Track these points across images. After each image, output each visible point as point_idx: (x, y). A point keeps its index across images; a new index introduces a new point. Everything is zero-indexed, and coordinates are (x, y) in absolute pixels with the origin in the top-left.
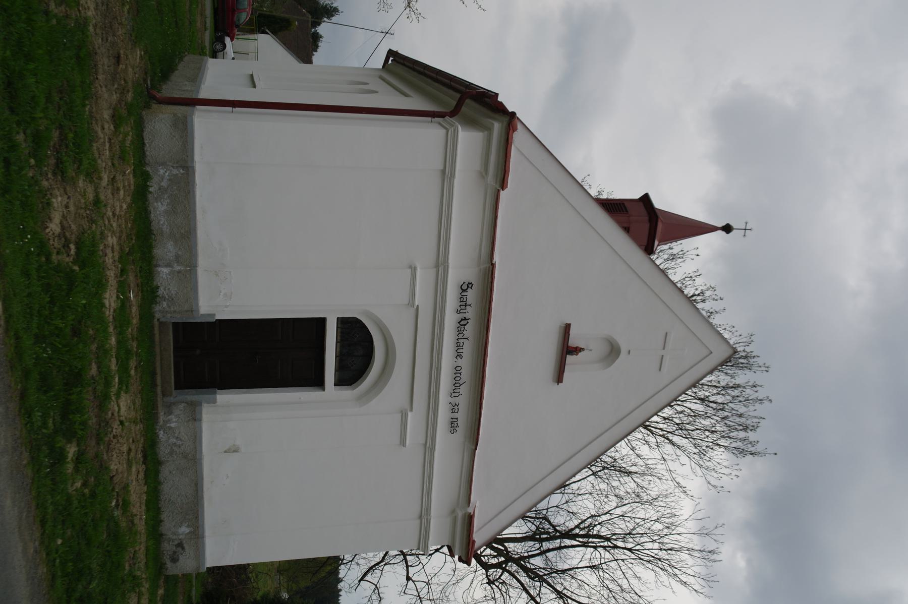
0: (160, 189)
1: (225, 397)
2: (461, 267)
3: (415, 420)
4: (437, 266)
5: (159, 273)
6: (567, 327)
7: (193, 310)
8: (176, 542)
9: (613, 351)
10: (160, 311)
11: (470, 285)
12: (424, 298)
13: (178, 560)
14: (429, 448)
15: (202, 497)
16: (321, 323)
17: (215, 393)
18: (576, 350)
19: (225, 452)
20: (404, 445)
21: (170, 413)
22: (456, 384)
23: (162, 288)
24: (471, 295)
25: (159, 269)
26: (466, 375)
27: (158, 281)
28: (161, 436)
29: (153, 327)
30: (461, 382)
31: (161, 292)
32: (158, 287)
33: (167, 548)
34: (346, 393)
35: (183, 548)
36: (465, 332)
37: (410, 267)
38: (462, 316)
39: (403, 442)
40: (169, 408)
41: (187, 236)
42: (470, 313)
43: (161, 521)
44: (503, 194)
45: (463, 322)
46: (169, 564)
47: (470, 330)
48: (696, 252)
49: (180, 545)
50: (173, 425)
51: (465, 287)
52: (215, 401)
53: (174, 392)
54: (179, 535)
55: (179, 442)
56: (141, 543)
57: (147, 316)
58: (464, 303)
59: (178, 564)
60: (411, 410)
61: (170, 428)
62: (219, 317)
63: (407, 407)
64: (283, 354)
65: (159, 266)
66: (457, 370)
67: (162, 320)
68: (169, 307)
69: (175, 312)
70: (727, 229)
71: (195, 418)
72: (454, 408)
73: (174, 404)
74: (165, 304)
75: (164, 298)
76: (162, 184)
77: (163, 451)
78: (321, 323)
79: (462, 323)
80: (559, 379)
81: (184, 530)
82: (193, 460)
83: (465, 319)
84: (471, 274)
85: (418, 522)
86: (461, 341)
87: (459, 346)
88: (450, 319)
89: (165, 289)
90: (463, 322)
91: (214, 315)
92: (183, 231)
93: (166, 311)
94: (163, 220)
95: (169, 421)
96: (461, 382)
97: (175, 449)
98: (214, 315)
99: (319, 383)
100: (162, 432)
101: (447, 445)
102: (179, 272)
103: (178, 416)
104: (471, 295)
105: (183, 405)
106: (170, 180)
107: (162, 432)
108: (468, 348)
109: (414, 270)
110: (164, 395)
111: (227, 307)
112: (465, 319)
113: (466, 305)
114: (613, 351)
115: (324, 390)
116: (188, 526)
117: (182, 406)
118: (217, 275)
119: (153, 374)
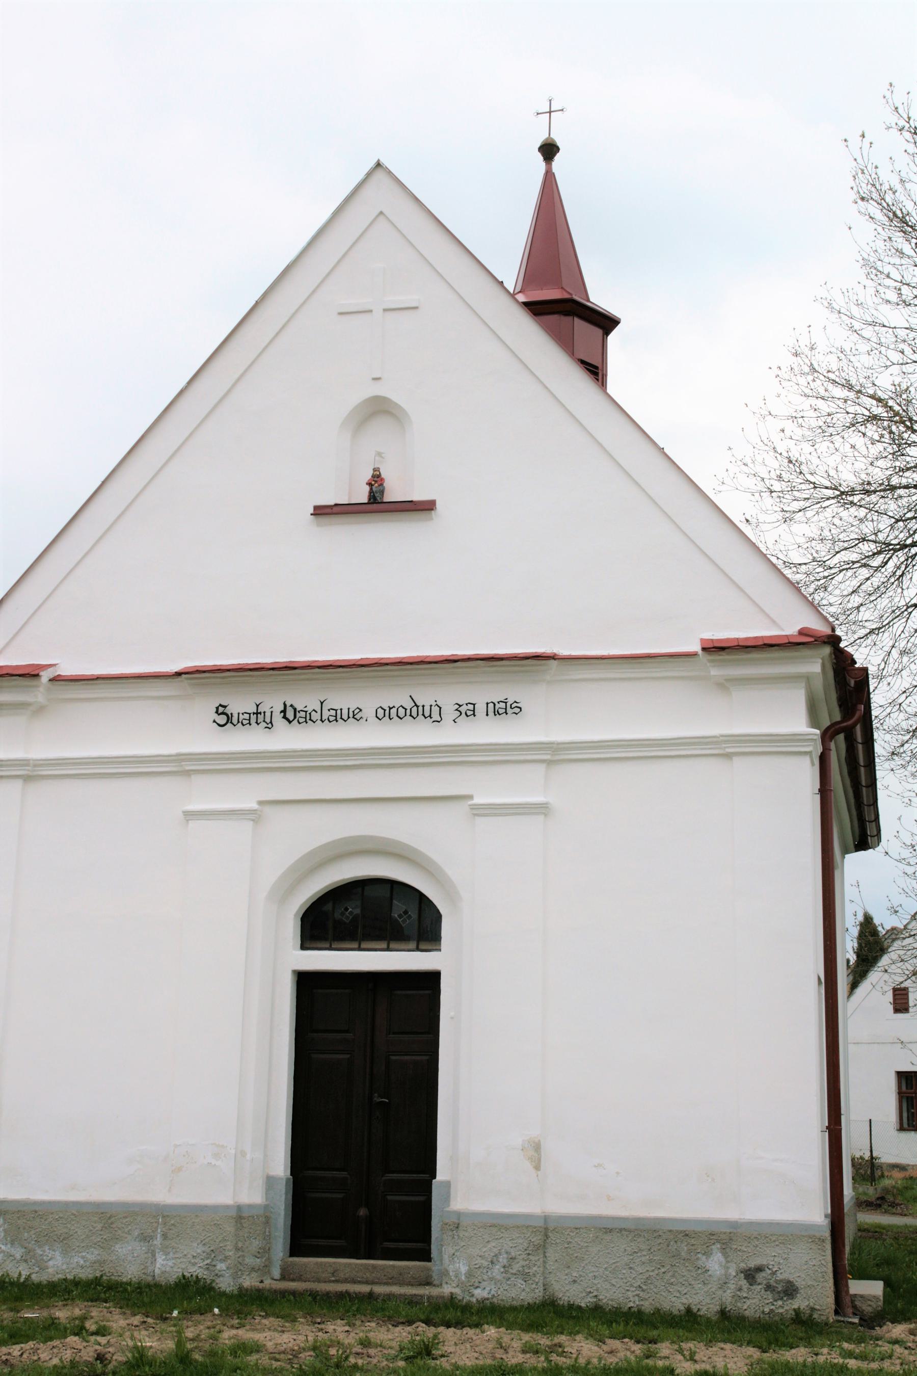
0: (26, 1261)
2: (189, 729)
5: (164, 1272)
6: (320, 512)
7: (265, 1217)
8: (744, 1283)
9: (378, 410)
10: (235, 1276)
11: (221, 710)
12: (244, 793)
13: (789, 1282)
14: (554, 755)
15: (638, 1220)
16: (307, 983)
18: (376, 482)
19: (537, 1168)
22: (416, 712)
24: (239, 705)
25: (157, 1271)
26: (398, 697)
28: (485, 1294)
30: (409, 704)
33: (756, 1303)
35: (759, 1269)
36: (309, 709)
39: (542, 809)
41: (108, 1219)
42: (273, 703)
43: (689, 1310)
46: (800, 1303)
47: (305, 700)
48: (855, 141)
49: (751, 1275)
50: (464, 1269)
51: (222, 720)
52: (447, 1185)
54: (727, 1276)
55: (503, 1259)
56: (366, 1343)
58: (257, 717)
59: (799, 1283)
60: (471, 797)
61: (469, 1274)
64: (365, 1060)
66: (386, 714)
68: (226, 1258)
70: (549, 150)
71: (456, 1225)
72: (467, 712)
74: (221, 1266)
75: (209, 1267)
76: (18, 1256)
77: (522, 1292)
78: (307, 983)
79: (291, 715)
80: (427, 507)
81: (715, 1263)
82: (545, 1233)
83: (284, 711)
84: (203, 709)
85: (736, 760)
87: (337, 717)
88: (287, 739)
89: (194, 1264)
92: (99, 1226)
94: (77, 1260)
96: (409, 704)
97: (516, 1267)
99: (431, 980)
101: (550, 716)
102: (165, 1236)
104: (239, 705)
106: (12, 1244)
108: (342, 700)
109: (190, 815)
112: (284, 711)
114: (378, 410)
116: (708, 1254)
118: (179, 1169)
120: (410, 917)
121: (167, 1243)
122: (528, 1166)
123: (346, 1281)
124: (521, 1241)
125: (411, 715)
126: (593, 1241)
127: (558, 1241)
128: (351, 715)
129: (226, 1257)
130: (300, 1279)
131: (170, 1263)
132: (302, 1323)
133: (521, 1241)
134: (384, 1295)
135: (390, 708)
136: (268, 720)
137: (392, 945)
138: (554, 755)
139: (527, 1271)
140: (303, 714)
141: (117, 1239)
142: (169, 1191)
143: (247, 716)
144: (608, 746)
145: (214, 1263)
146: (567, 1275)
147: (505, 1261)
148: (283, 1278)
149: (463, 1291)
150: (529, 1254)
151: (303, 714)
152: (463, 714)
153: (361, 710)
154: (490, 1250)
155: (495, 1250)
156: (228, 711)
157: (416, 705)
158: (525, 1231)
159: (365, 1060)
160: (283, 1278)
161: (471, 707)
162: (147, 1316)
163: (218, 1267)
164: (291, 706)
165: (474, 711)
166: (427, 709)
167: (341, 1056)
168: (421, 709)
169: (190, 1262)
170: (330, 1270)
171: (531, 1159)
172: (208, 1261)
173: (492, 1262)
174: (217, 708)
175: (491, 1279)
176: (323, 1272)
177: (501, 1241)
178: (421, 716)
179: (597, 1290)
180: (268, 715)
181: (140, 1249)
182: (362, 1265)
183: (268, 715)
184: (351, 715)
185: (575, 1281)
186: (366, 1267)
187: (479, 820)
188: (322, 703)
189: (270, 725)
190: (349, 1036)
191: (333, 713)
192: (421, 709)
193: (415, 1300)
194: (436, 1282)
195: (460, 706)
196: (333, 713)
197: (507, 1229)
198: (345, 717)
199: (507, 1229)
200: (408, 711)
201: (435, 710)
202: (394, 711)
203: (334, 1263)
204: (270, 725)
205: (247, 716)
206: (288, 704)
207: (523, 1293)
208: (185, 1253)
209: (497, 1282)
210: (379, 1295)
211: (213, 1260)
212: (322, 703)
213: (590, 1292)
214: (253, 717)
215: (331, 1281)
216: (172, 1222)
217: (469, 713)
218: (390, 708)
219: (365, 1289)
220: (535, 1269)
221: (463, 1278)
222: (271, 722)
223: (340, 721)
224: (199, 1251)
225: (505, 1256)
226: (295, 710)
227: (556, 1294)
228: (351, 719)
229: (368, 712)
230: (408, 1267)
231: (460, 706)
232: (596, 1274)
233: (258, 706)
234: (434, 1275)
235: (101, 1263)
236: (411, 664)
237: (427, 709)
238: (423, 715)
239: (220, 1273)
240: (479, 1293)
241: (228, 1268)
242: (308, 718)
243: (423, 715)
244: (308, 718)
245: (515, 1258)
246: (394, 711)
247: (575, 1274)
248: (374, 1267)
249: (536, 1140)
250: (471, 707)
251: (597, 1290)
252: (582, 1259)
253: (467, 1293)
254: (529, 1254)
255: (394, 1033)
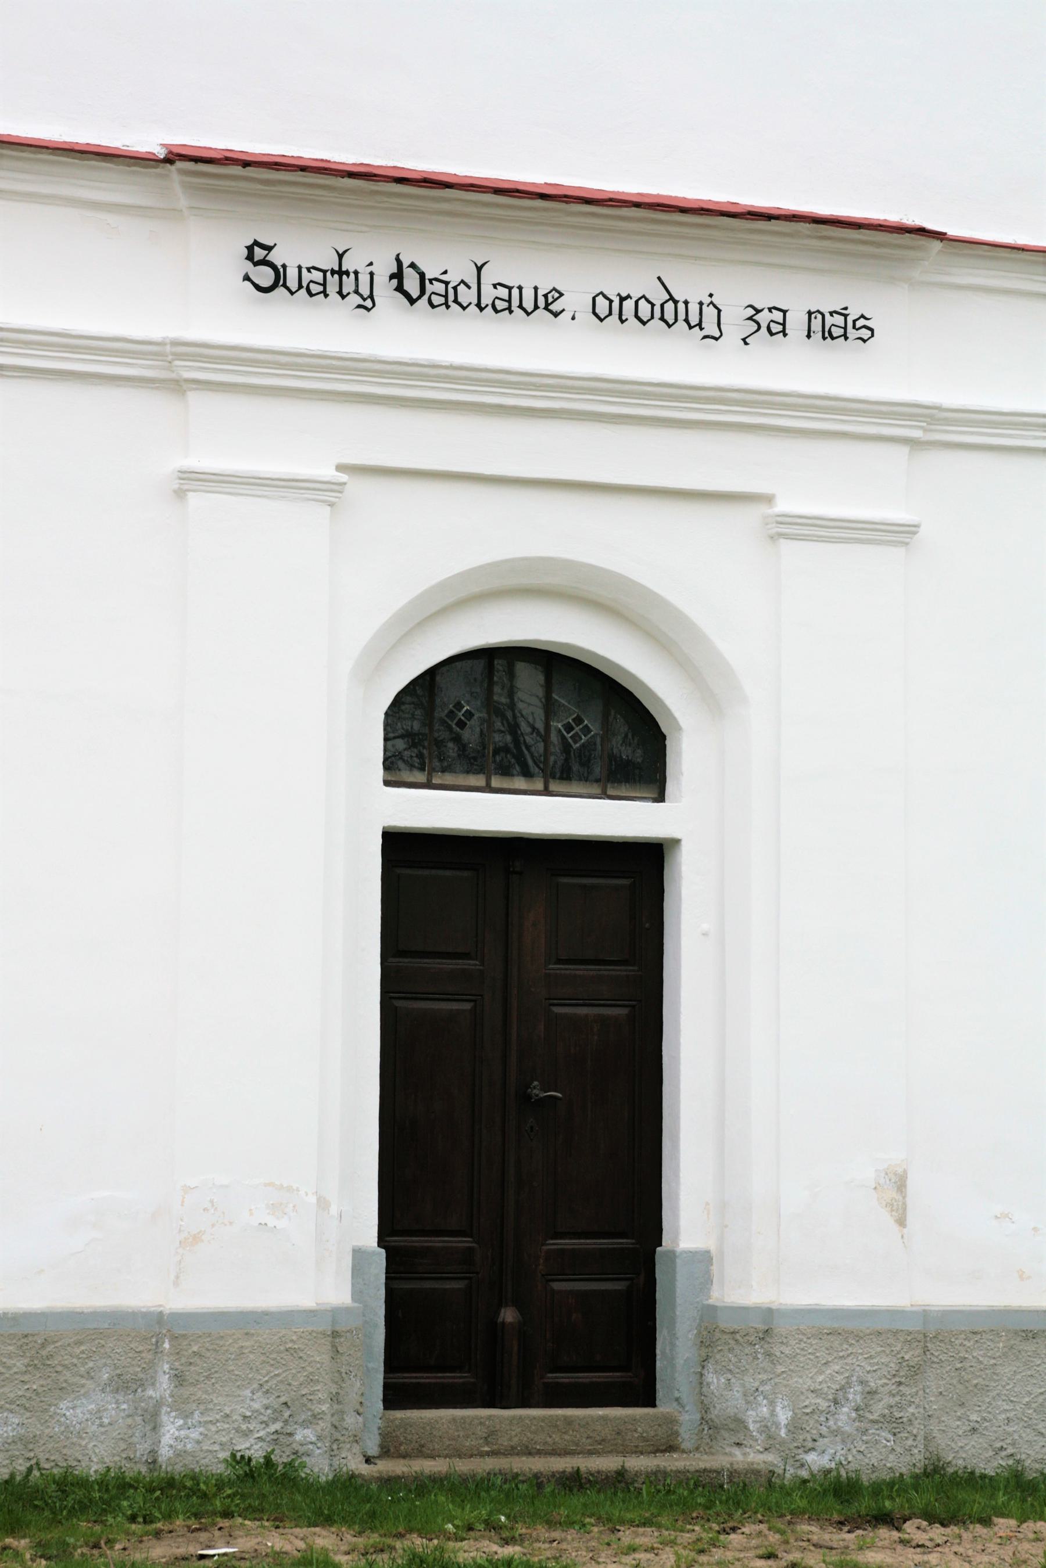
1: (690, 1217)
2: (181, 286)
3: (808, 481)
4: (178, 387)
7: (333, 1331)
11: (257, 253)
12: (309, 442)
14: (927, 430)
16: (401, 848)
17: (672, 1255)
19: (901, 1222)
20: (910, 530)
21: (739, 1424)
22: (668, 313)
23: (242, 1446)
24: (300, 249)
25: (165, 1453)
26: (633, 277)
27: (213, 1461)
29: (389, 1482)
30: (659, 296)
31: (257, 1453)
32: (238, 1460)
34: (689, 758)
36: (453, 278)
37: (180, 494)
38: (384, 289)
39: (900, 535)
40: (712, 1428)
42: (372, 254)
44: (952, 231)
45: (412, 285)
47: (443, 258)
50: (784, 1416)
51: (264, 275)
52: (704, 1258)
53: (664, 1407)
55: (855, 1395)
57: (342, 1501)
58: (336, 280)
60: (768, 499)
61: (795, 1427)
62: (366, 1229)
63: (751, 516)
64: (523, 1016)
65: (153, 1452)
66: (611, 309)
67: (373, 1447)
69: (335, 1398)
71: (719, 1334)
73: (705, 1409)
74: (304, 1434)
78: (401, 848)
79: (412, 287)
86: (489, 294)
87: (509, 303)
88: (399, 334)
89: (246, 1434)
90: (412, 285)
91: (358, 1253)
92: (19, 1364)
93: (341, 1426)
95: (767, 1428)
96: (659, 296)
97: (879, 1409)
98: (358, 1253)
99: (644, 866)
100: (811, 1458)
102: (179, 1379)
103: (751, 1396)
104: (300, 249)
105: (710, 1377)
106: (216, 1485)
107: (811, 1458)
108: (520, 266)
109: (191, 481)
110: (671, 1448)
111: (323, 1204)
112: (398, 276)
113: (341, 273)
115: (676, 842)
117: (714, 1380)
118: (196, 1238)
119: (574, 1482)
120: (587, 730)
121: (185, 1392)
122: (888, 1220)
123: (512, 1452)
124: (885, 1359)
125: (662, 319)
126: (1005, 1354)
127: (943, 1357)
128: (541, 302)
129: (314, 1416)
130: (421, 1452)
131: (195, 1435)
132: (242, 1537)
133: (885, 1359)
134: (648, 1475)
135: (622, 299)
136: (365, 290)
137: (553, 786)
138: (927, 430)
139: (897, 1415)
140: (440, 288)
141: (63, 1390)
142: (176, 1283)
143: (318, 276)
144: (1025, 424)
145: (289, 1429)
146: (959, 1419)
147: (858, 1398)
148: (386, 1452)
149: (785, 1460)
150: (900, 1383)
151: (440, 288)
152: (764, 329)
153: (561, 295)
154: (832, 1378)
155: (839, 1378)
156: (275, 257)
157: (672, 298)
158: (891, 1341)
159: (523, 1016)
160: (386, 1452)
161: (778, 316)
162: (841, 1562)
163: (298, 1437)
164: (413, 266)
165: (784, 324)
166: (694, 308)
167: (455, 1006)
168: (681, 307)
169: (237, 1430)
170: (481, 1431)
171: (890, 1206)
172: (277, 1426)
173: (836, 1402)
174: (250, 249)
175: (836, 1432)
176: (467, 1437)
177: (849, 1360)
178: (681, 324)
179: (1013, 1444)
180: (364, 279)
181: (115, 1409)
182: (543, 1419)
183: (364, 279)
184: (541, 302)
185: (974, 1430)
186: (553, 1424)
187: (784, 544)
188: (479, 269)
189: (368, 303)
190: (472, 964)
191: (503, 293)
192: (681, 307)
193: (704, 1479)
194: (686, 1445)
195: (758, 311)
196: (503, 293)
197: (858, 1338)
198: (529, 305)
199: (858, 1338)
200: (657, 309)
201: (710, 313)
202: (628, 305)
203: (489, 1418)
204: (368, 303)
205: (318, 276)
206: (406, 263)
207: (892, 1457)
208: (227, 1411)
209: (845, 1438)
210: (637, 1474)
211: (286, 1422)
212: (479, 269)
213: (1002, 1448)
214: (333, 281)
215: (482, 1455)
216: (195, 1349)
217: (775, 328)
218: (622, 299)
219: (608, 1463)
220: (911, 1410)
221: (783, 1433)
222: (371, 296)
223: (518, 312)
224: (256, 1406)
225: (859, 1388)
226: (422, 276)
227: (942, 1454)
228: (541, 312)
229: (576, 300)
230: (634, 1420)
231: (758, 311)
232: (1011, 1415)
233: (341, 256)
234: (682, 1431)
235: (26, 1442)
236: (684, 210)
237: (694, 308)
238: (686, 320)
239: (302, 1450)
240: (817, 1461)
241: (319, 1438)
242: (450, 299)
243: (686, 320)
244: (451, 297)
245: (875, 1392)
246: (628, 305)
247: (974, 1417)
248: (569, 1421)
249: (900, 1171)
250: (778, 316)
251: (1013, 1444)
252: (985, 1389)
253: (790, 1461)
254: (900, 1383)
255: (559, 961)
